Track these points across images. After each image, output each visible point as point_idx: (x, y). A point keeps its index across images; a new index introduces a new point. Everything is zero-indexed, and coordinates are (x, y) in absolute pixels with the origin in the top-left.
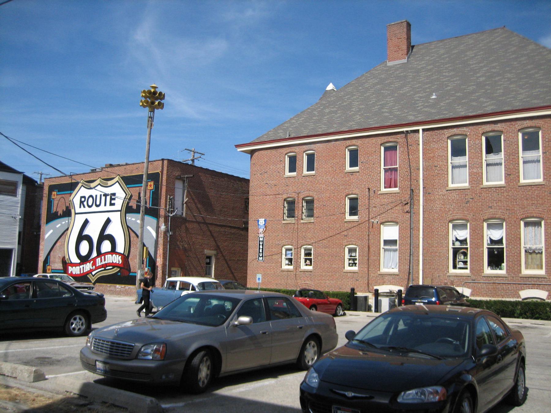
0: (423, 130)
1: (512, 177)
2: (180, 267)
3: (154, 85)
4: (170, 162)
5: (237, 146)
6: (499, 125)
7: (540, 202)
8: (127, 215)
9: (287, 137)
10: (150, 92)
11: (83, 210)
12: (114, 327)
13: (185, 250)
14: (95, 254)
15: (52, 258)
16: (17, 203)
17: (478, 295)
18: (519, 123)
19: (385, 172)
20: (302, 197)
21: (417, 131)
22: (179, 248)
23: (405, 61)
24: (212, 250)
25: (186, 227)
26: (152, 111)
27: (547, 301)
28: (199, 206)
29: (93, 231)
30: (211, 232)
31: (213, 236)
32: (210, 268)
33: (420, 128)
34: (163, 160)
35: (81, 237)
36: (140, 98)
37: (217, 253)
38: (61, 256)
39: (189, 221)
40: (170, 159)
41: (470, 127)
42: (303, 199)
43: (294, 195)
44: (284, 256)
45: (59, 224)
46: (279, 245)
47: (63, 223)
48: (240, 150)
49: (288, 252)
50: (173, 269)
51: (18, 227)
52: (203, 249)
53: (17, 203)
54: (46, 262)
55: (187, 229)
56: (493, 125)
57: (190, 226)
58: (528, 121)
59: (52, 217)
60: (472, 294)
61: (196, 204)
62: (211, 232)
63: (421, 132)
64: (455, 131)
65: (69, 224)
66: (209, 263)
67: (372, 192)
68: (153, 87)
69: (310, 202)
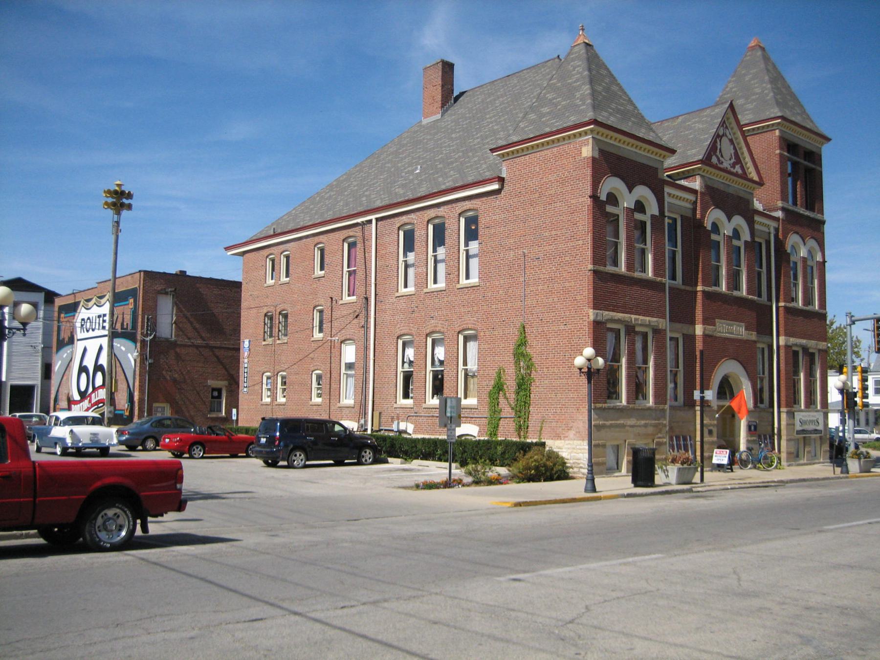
0: (377, 220)
1: (451, 276)
2: (167, 402)
3: (118, 182)
4: (145, 272)
5: (227, 249)
6: (442, 209)
7: (475, 309)
8: (115, 340)
9: (272, 233)
10: (116, 192)
11: (86, 335)
12: (861, 522)
13: (175, 381)
14: (91, 389)
15: (60, 397)
16: (39, 329)
17: (420, 433)
18: (460, 204)
19: (350, 275)
20: (278, 311)
21: (370, 221)
22: (165, 378)
23: (439, 116)
24: (221, 380)
25: (176, 353)
26: (118, 213)
27: (414, 436)
28: (197, 326)
29: (90, 363)
30: (217, 357)
31: (222, 363)
32: (220, 404)
33: (373, 217)
34: (140, 271)
35: (83, 369)
36: (104, 198)
37: (230, 384)
38: (66, 392)
39: (181, 346)
40: (149, 270)
41: (418, 213)
42: (280, 313)
43: (272, 309)
44: (264, 386)
45: (65, 353)
46: (259, 372)
47: (123, 348)
48: (230, 253)
49: (269, 381)
50: (155, 405)
51: (40, 358)
52: (206, 379)
53: (39, 329)
54: (56, 400)
55: (178, 357)
56: (436, 209)
57: (182, 351)
58: (467, 202)
59: (61, 345)
60: (415, 432)
61: (191, 323)
62: (217, 357)
63: (374, 222)
64: (404, 219)
65: (72, 352)
66: (219, 397)
67: (334, 302)
68: (118, 185)
69: (286, 316)
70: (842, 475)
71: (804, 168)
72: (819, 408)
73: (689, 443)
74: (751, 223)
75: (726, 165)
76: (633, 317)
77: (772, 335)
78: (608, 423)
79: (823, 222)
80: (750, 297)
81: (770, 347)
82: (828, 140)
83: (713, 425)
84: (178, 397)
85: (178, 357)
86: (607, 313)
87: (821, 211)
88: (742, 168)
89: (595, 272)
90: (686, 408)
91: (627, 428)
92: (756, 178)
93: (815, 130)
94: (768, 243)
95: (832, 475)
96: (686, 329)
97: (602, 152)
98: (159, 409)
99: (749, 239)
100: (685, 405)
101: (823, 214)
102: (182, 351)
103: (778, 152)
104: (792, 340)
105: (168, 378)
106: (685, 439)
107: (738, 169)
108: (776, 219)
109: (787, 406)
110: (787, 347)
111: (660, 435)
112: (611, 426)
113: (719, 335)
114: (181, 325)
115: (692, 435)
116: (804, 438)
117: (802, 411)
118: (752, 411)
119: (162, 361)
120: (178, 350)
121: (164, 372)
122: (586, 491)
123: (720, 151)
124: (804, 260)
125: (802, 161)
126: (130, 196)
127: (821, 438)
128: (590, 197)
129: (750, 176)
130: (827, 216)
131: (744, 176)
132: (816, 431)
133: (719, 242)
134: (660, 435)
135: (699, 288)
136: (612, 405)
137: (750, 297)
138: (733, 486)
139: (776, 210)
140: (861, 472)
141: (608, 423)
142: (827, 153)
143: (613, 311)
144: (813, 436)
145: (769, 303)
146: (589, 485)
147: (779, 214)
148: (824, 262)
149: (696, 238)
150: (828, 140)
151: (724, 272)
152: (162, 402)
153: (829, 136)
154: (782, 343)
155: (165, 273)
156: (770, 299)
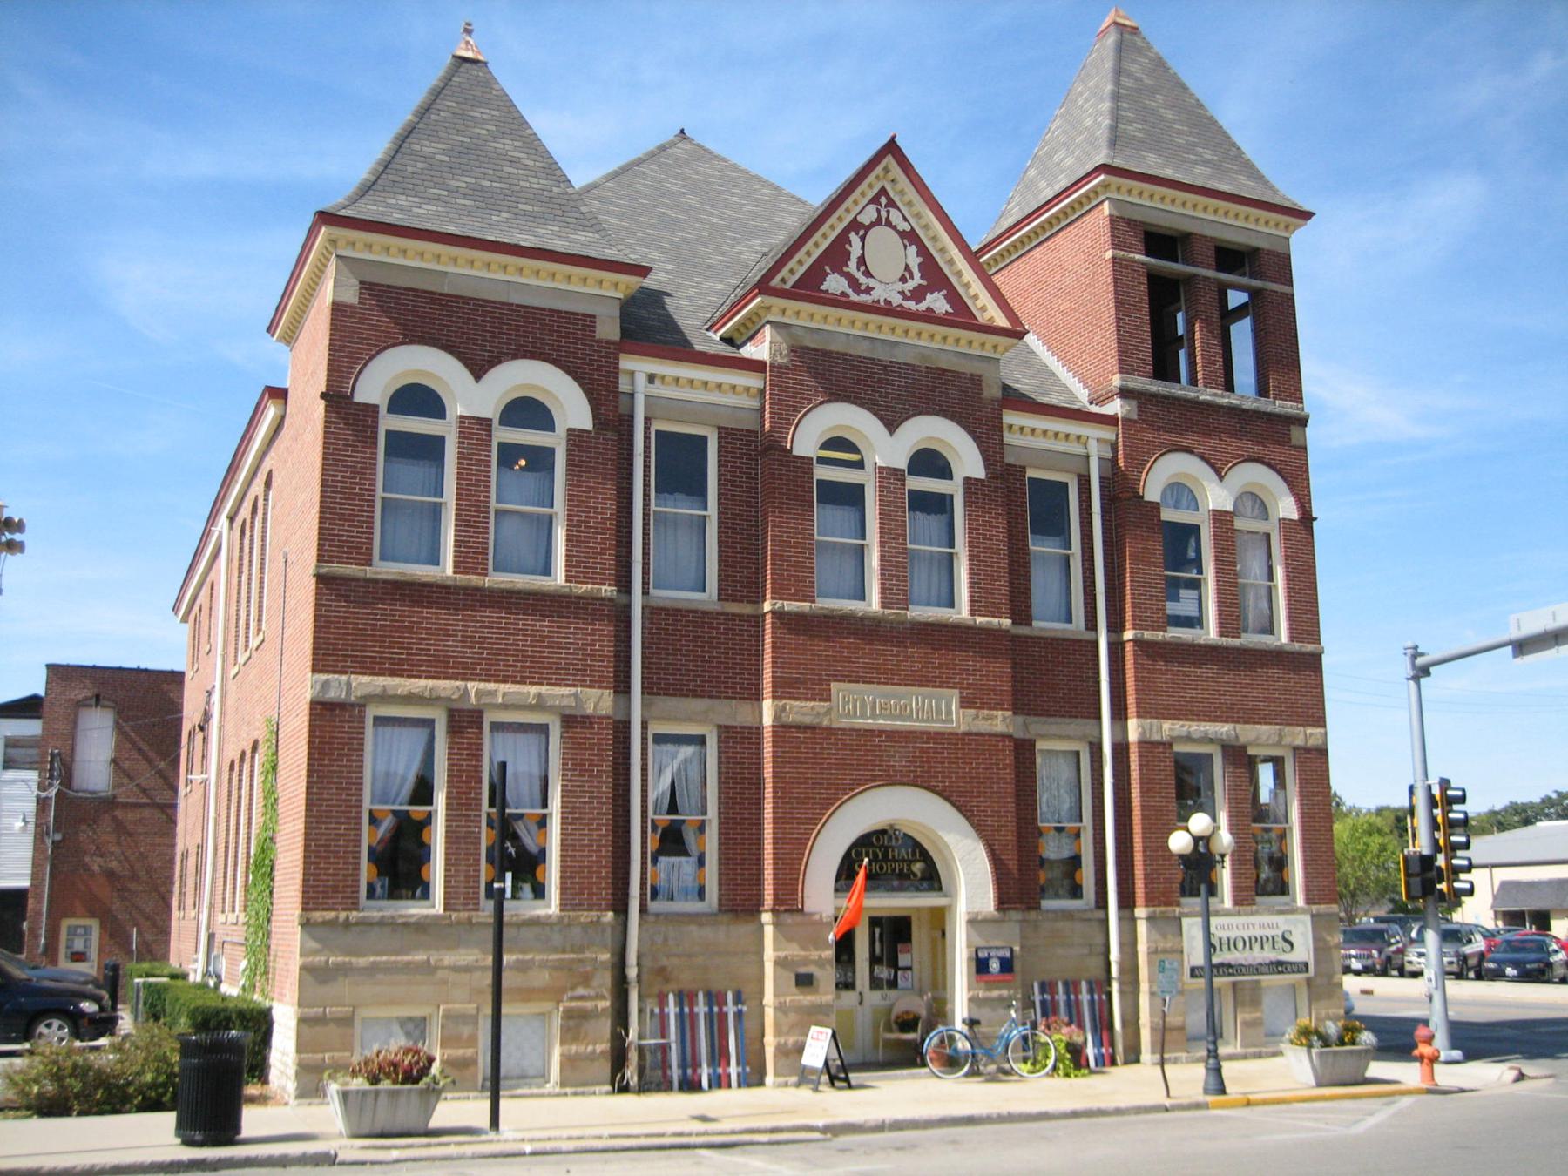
2: (93, 915)
13: (110, 875)
22: (87, 869)
25: (114, 818)
39: (125, 806)
55: (119, 827)
57: (129, 816)
70: (1210, 1099)
71: (1205, 291)
72: (1300, 901)
73: (730, 1009)
74: (988, 437)
75: (887, 290)
76: (473, 687)
77: (1099, 717)
78: (362, 961)
79: (1303, 422)
80: (979, 620)
81: (1096, 749)
82: (1307, 215)
83: (820, 963)
84: (117, 905)
85: (119, 827)
86: (365, 679)
87: (1296, 395)
88: (954, 297)
89: (321, 579)
90: (725, 918)
91: (440, 974)
92: (1002, 321)
93: (1277, 201)
94: (1084, 482)
95: (1159, 1097)
96: (738, 713)
97: (367, 287)
98: (80, 931)
99: (979, 472)
100: (722, 909)
101: (1300, 400)
102: (129, 816)
103: (1109, 254)
104: (1168, 728)
105: (96, 868)
106: (715, 998)
107: (937, 302)
108: (1110, 420)
109: (1149, 902)
110: (1145, 745)
111: (581, 991)
112: (373, 969)
113: (845, 722)
114: (126, 765)
115: (747, 991)
116: (1234, 984)
117: (1227, 913)
118: (987, 921)
119: (83, 836)
120: (118, 813)
121: (87, 859)
122: (1206, 1091)
123: (862, 261)
124: (1222, 520)
125: (1211, 273)
126: (19, 527)
127: (1309, 981)
128: (323, 396)
129: (982, 319)
130: (1309, 406)
131: (961, 316)
132: (1278, 967)
133: (862, 487)
134: (581, 991)
135: (767, 607)
136: (387, 913)
137: (979, 620)
138: (539, 1146)
139: (1109, 398)
140: (1319, 1085)
141: (362, 961)
142: (1304, 247)
143: (393, 674)
144: (1267, 980)
145: (1089, 636)
146: (1212, 1080)
147: (1116, 407)
148: (1307, 519)
149: (763, 484)
150: (1307, 215)
151: (874, 560)
152: (83, 916)
153: (1306, 207)
154: (1133, 736)
155: (120, 669)
156: (1091, 624)
